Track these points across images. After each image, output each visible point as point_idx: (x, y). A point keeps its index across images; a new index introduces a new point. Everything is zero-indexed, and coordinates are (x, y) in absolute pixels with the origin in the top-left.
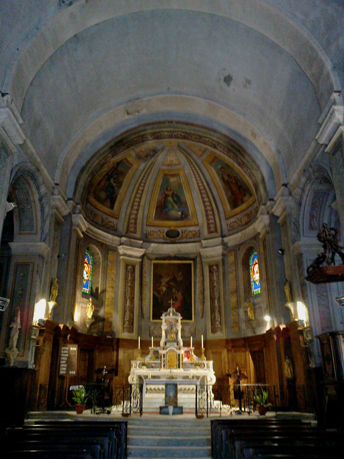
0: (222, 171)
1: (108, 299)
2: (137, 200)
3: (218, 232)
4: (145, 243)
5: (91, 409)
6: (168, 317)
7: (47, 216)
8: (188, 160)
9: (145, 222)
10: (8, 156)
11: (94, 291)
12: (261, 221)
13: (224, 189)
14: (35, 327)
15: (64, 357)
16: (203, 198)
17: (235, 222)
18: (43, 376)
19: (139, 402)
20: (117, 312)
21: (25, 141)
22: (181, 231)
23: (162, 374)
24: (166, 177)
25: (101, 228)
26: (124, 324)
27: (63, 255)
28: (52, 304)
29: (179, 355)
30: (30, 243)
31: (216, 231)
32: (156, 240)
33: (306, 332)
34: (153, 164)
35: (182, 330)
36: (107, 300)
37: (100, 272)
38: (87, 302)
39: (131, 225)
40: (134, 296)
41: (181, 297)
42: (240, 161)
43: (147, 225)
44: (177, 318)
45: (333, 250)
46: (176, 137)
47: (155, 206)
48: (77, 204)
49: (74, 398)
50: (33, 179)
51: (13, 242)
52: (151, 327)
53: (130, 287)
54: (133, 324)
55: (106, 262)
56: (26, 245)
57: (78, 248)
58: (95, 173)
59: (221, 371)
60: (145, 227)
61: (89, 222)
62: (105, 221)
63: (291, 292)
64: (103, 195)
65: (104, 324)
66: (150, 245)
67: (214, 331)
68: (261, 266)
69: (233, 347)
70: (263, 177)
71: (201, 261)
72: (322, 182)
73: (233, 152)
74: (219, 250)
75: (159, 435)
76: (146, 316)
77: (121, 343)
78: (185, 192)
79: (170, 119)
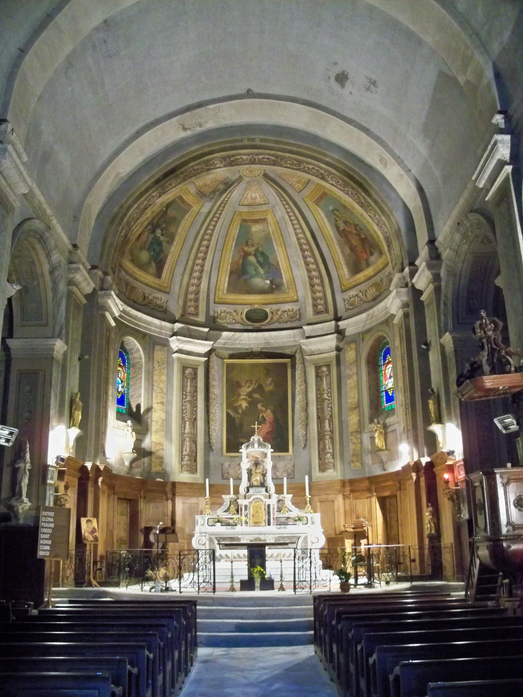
1: (157, 422)
2: (199, 261)
3: (330, 312)
4: (211, 332)
5: (141, 585)
6: (250, 449)
8: (280, 196)
10: (8, 213)
11: (134, 410)
13: (339, 243)
14: (52, 467)
15: (46, 528)
16: (305, 257)
17: (357, 295)
20: (171, 441)
24: (245, 224)
26: (182, 460)
28: (75, 432)
29: (269, 506)
31: (327, 311)
32: (230, 326)
34: (224, 204)
35: (274, 467)
36: (154, 423)
37: (143, 380)
39: (189, 303)
43: (215, 303)
44: (264, 450)
46: (261, 162)
47: (229, 270)
48: (106, 274)
50: (41, 243)
52: (224, 464)
54: (195, 460)
55: (151, 363)
58: (133, 223)
59: (333, 527)
64: (145, 256)
65: (151, 460)
66: (221, 335)
67: (323, 468)
68: (396, 367)
69: (352, 491)
71: (303, 359)
72: (485, 240)
74: (331, 341)
77: (177, 490)
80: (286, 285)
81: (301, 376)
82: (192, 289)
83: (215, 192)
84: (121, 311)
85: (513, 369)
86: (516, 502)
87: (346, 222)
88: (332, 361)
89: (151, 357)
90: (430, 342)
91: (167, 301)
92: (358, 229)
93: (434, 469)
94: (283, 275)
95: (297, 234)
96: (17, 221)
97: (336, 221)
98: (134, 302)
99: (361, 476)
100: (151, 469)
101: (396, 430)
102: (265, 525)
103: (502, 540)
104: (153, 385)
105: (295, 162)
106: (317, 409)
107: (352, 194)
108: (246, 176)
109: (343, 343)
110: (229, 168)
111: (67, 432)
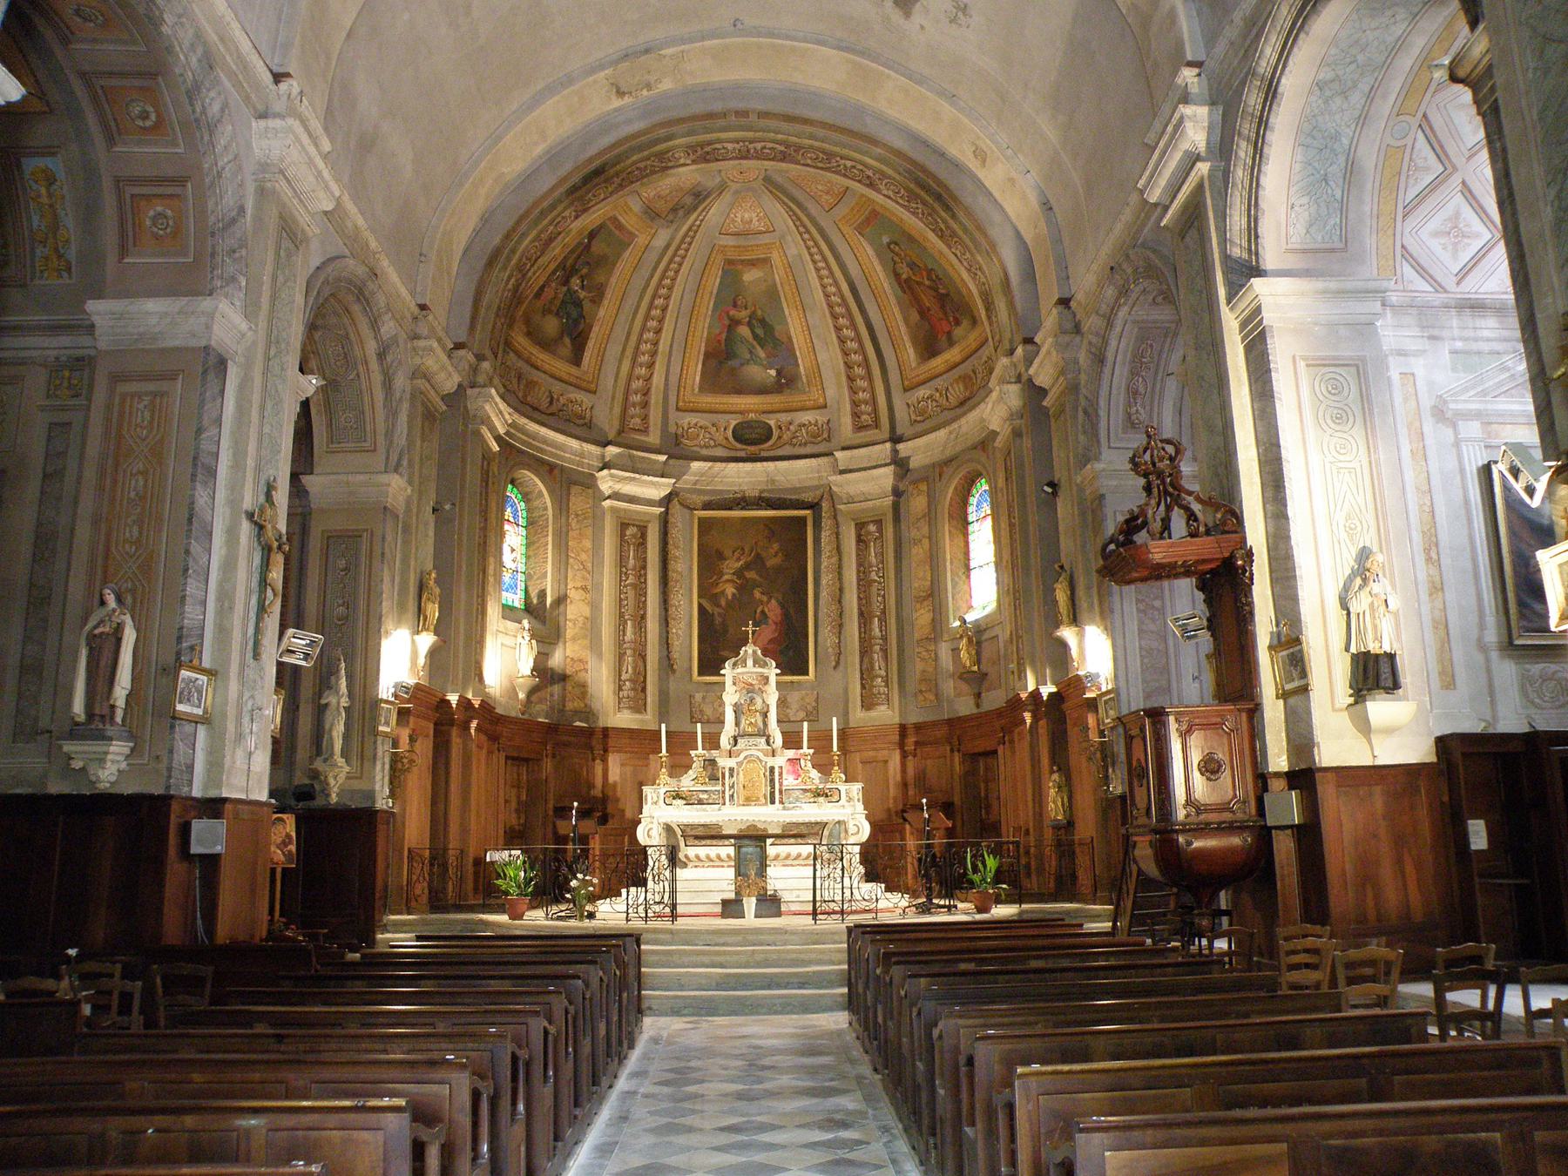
0: (893, 251)
1: (574, 622)
2: (649, 335)
4: (672, 462)
6: (740, 670)
11: (535, 601)
12: (1000, 399)
14: (387, 702)
16: (838, 329)
17: (930, 397)
18: (415, 830)
19: (667, 889)
20: (600, 655)
21: (338, 201)
24: (732, 270)
25: (551, 420)
26: (620, 689)
27: (447, 507)
28: (427, 640)
29: (772, 769)
30: (361, 477)
31: (877, 425)
32: (705, 452)
33: (1106, 702)
34: (693, 231)
35: (782, 703)
37: (550, 547)
38: (517, 631)
39: (632, 411)
40: (645, 613)
41: (778, 611)
42: (943, 227)
43: (678, 409)
46: (759, 156)
48: (480, 357)
49: (499, 882)
51: (312, 473)
53: (634, 586)
54: (644, 690)
56: (348, 483)
60: (673, 415)
62: (558, 400)
63: (1072, 599)
64: (551, 325)
67: (868, 703)
70: (1006, 274)
71: (835, 510)
72: (1159, 299)
74: (885, 478)
75: (722, 966)
77: (611, 742)
78: (787, 313)
79: (742, 106)
84: (509, 425)
85: (1202, 529)
86: (1202, 764)
87: (912, 265)
95: (824, 287)
96: (316, 261)
98: (535, 409)
101: (997, 636)
102: (766, 804)
103: (1177, 831)
106: (860, 599)
111: (413, 642)
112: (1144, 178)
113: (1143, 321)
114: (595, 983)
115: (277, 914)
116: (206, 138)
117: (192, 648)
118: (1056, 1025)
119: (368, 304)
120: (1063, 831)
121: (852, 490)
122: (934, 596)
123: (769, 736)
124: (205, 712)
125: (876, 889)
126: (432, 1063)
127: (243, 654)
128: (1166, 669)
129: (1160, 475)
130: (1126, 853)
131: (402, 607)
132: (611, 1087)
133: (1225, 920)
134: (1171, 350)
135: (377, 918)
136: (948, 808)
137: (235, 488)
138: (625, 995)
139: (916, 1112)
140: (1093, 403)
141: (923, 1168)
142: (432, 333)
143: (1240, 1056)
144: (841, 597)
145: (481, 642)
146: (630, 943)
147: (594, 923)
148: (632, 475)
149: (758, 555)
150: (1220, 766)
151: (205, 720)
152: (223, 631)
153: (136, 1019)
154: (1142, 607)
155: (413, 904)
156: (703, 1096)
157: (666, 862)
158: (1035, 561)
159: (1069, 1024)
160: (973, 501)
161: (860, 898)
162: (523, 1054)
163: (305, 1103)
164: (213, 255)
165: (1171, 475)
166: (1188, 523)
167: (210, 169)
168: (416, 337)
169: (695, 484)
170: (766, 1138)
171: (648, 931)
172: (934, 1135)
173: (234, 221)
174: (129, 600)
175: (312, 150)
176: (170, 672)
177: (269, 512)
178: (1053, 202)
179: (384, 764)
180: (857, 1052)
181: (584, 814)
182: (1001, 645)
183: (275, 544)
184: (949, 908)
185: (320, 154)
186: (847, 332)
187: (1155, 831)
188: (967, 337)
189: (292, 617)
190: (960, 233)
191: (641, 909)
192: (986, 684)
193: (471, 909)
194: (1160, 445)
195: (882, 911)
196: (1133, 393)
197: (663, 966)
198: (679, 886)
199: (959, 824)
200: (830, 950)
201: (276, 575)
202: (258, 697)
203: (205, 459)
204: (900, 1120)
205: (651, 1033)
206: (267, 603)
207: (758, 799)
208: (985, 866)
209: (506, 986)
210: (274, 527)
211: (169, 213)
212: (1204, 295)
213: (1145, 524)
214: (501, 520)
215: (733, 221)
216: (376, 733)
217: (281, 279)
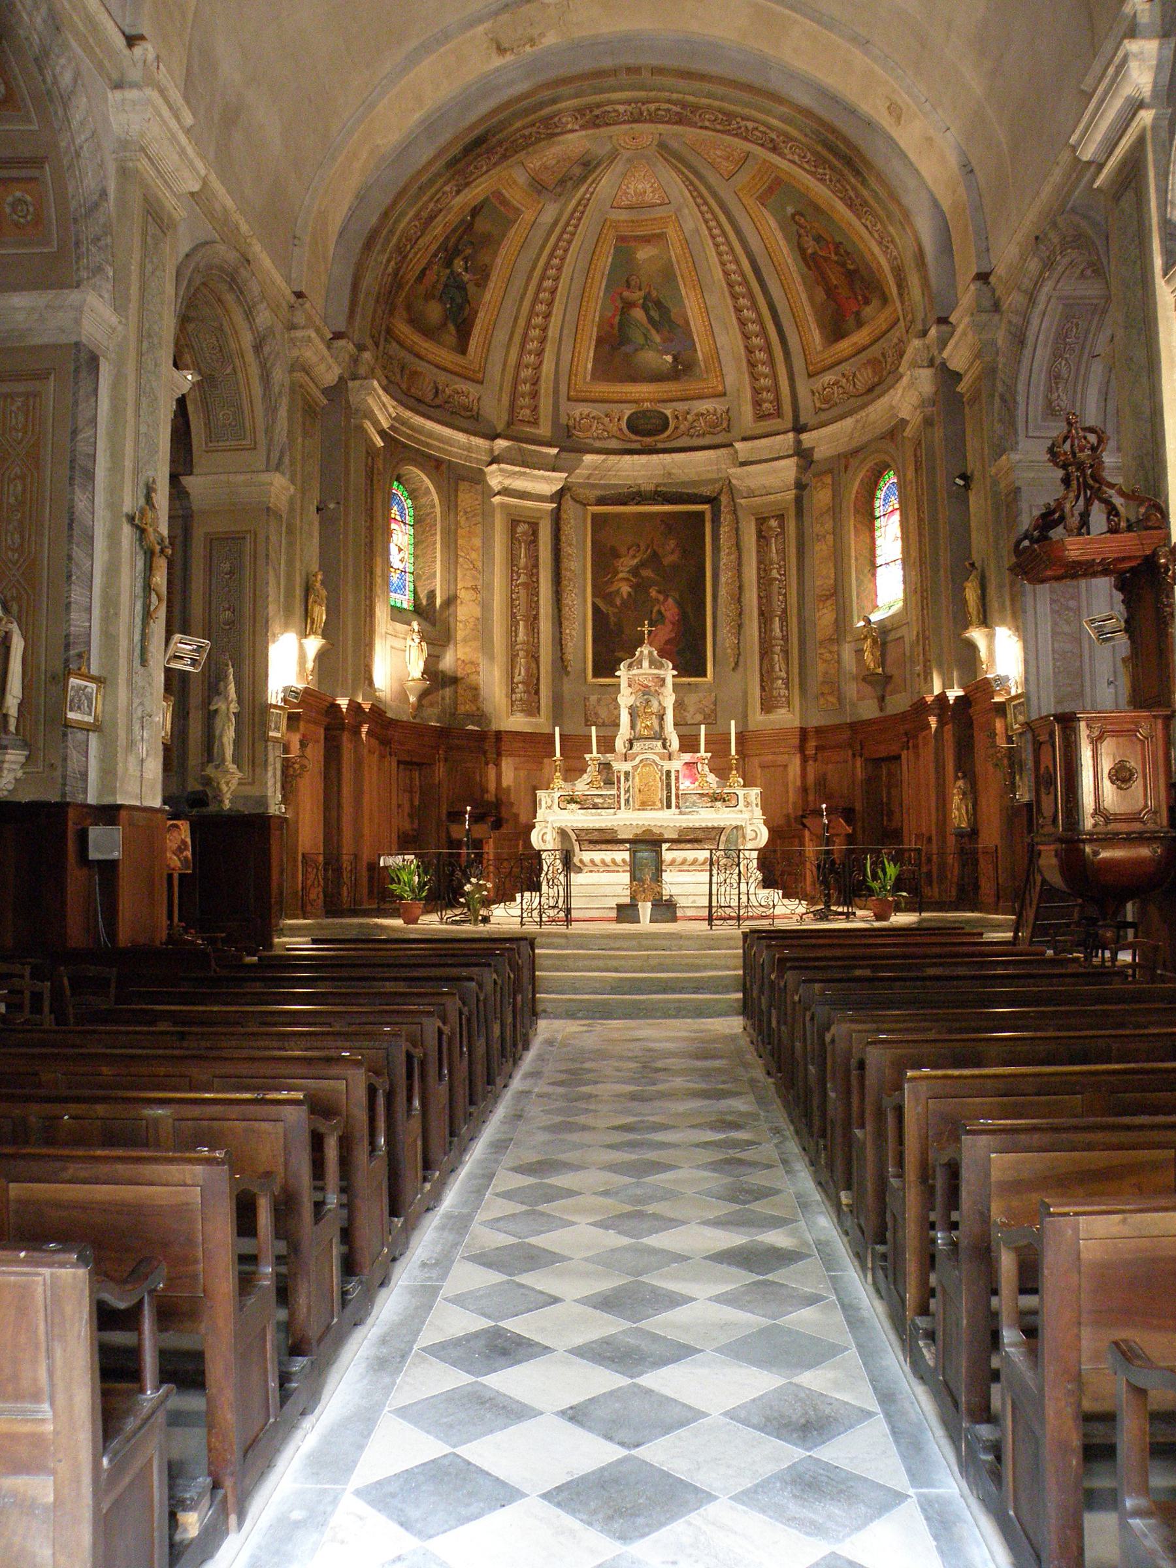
0: (796, 223)
1: (466, 622)
2: (538, 320)
4: (564, 455)
6: (635, 671)
7: (280, 393)
8: (691, 188)
9: (563, 388)
11: (424, 602)
12: (912, 384)
14: (276, 707)
16: (738, 310)
17: (836, 383)
19: (561, 893)
20: (492, 658)
21: (205, 182)
22: (673, 413)
23: (622, 823)
24: (625, 246)
26: (513, 692)
28: (314, 644)
29: (668, 773)
30: (242, 478)
31: (779, 414)
34: (583, 203)
35: (679, 706)
37: (438, 546)
39: (522, 402)
42: (852, 194)
43: (569, 399)
45: (1089, 492)
46: (653, 119)
47: (594, 337)
48: (361, 348)
49: (393, 887)
51: (191, 474)
54: (537, 692)
55: (452, 516)
57: (372, 481)
61: (396, 400)
62: (444, 391)
63: (983, 597)
64: (434, 312)
72: (1088, 272)
73: (832, 168)
74: (787, 470)
75: (616, 970)
76: (573, 665)
77: (504, 746)
78: (683, 292)
79: (631, 61)
80: (702, 364)
81: (729, 537)
82: (526, 373)
83: (565, 182)
84: (394, 419)
85: (1123, 524)
86: (1113, 772)
87: (818, 239)
88: (787, 509)
89: (452, 504)
90: (972, 473)
91: (479, 399)
92: (842, 251)
93: (971, 711)
94: (698, 345)
95: (723, 264)
96: (185, 247)
97: (800, 236)
98: (419, 401)
99: (837, 721)
100: (456, 709)
101: (903, 637)
102: (662, 808)
103: (1084, 841)
104: (457, 556)
105: (720, 116)
106: (760, 597)
107: (831, 181)
108: (624, 148)
109: (809, 474)
110: (590, 132)
111: (301, 646)
112: (1078, 132)
113: (1068, 298)
114: (489, 988)
115: (176, 919)
116: (60, 113)
117: (80, 656)
118: (950, 1031)
119: (242, 293)
120: (966, 840)
121: (753, 483)
122: (838, 594)
123: (665, 740)
124: (96, 719)
125: (776, 895)
126: (328, 1060)
127: (130, 661)
128: (1080, 674)
129: (1080, 466)
130: (1031, 861)
131: (288, 611)
132: (505, 1086)
133: (1130, 932)
134: (1099, 328)
135: (273, 921)
136: (848, 814)
137: (114, 490)
138: (519, 998)
139: (807, 1114)
140: (1012, 389)
141: (812, 1168)
142: (310, 323)
143: (1132, 1065)
144: (740, 594)
145: (370, 646)
146: (525, 947)
147: (488, 927)
148: (523, 470)
149: (655, 554)
150: (1132, 775)
151: (96, 727)
152: (109, 638)
153: (48, 1019)
154: (1056, 607)
155: (309, 908)
156: (597, 1096)
157: (560, 867)
158: (945, 558)
159: (961, 1030)
160: (880, 494)
161: (756, 904)
162: (418, 1053)
163: (207, 1095)
164: (77, 244)
165: (1091, 466)
166: (1108, 518)
167: (68, 147)
168: (292, 327)
169: (588, 478)
170: (660, 1137)
171: (542, 935)
172: (824, 1136)
173: (96, 205)
174: (15, 608)
175: (173, 124)
176: (60, 679)
177: (150, 514)
178: (974, 163)
179: (275, 769)
180: (751, 1057)
181: (476, 819)
182: (908, 649)
183: (158, 548)
184: (847, 915)
185: (182, 127)
186: (748, 314)
187: (1061, 840)
188: (876, 318)
189: (178, 624)
190: (871, 201)
191: (535, 913)
192: (890, 688)
193: (367, 913)
194: (1081, 434)
195: (779, 917)
196: (1055, 378)
197: (558, 970)
198: (574, 891)
199: (859, 831)
200: (725, 956)
201: (160, 579)
202: (147, 703)
203: (81, 461)
204: (792, 1122)
205: (546, 1035)
206: (152, 608)
207: (654, 804)
208: (885, 873)
209: (402, 988)
210: (156, 530)
211: (28, 198)
212: (1138, 267)
213: (1062, 518)
214: (388, 519)
215: (626, 193)
216: (266, 739)
217: (149, 267)
